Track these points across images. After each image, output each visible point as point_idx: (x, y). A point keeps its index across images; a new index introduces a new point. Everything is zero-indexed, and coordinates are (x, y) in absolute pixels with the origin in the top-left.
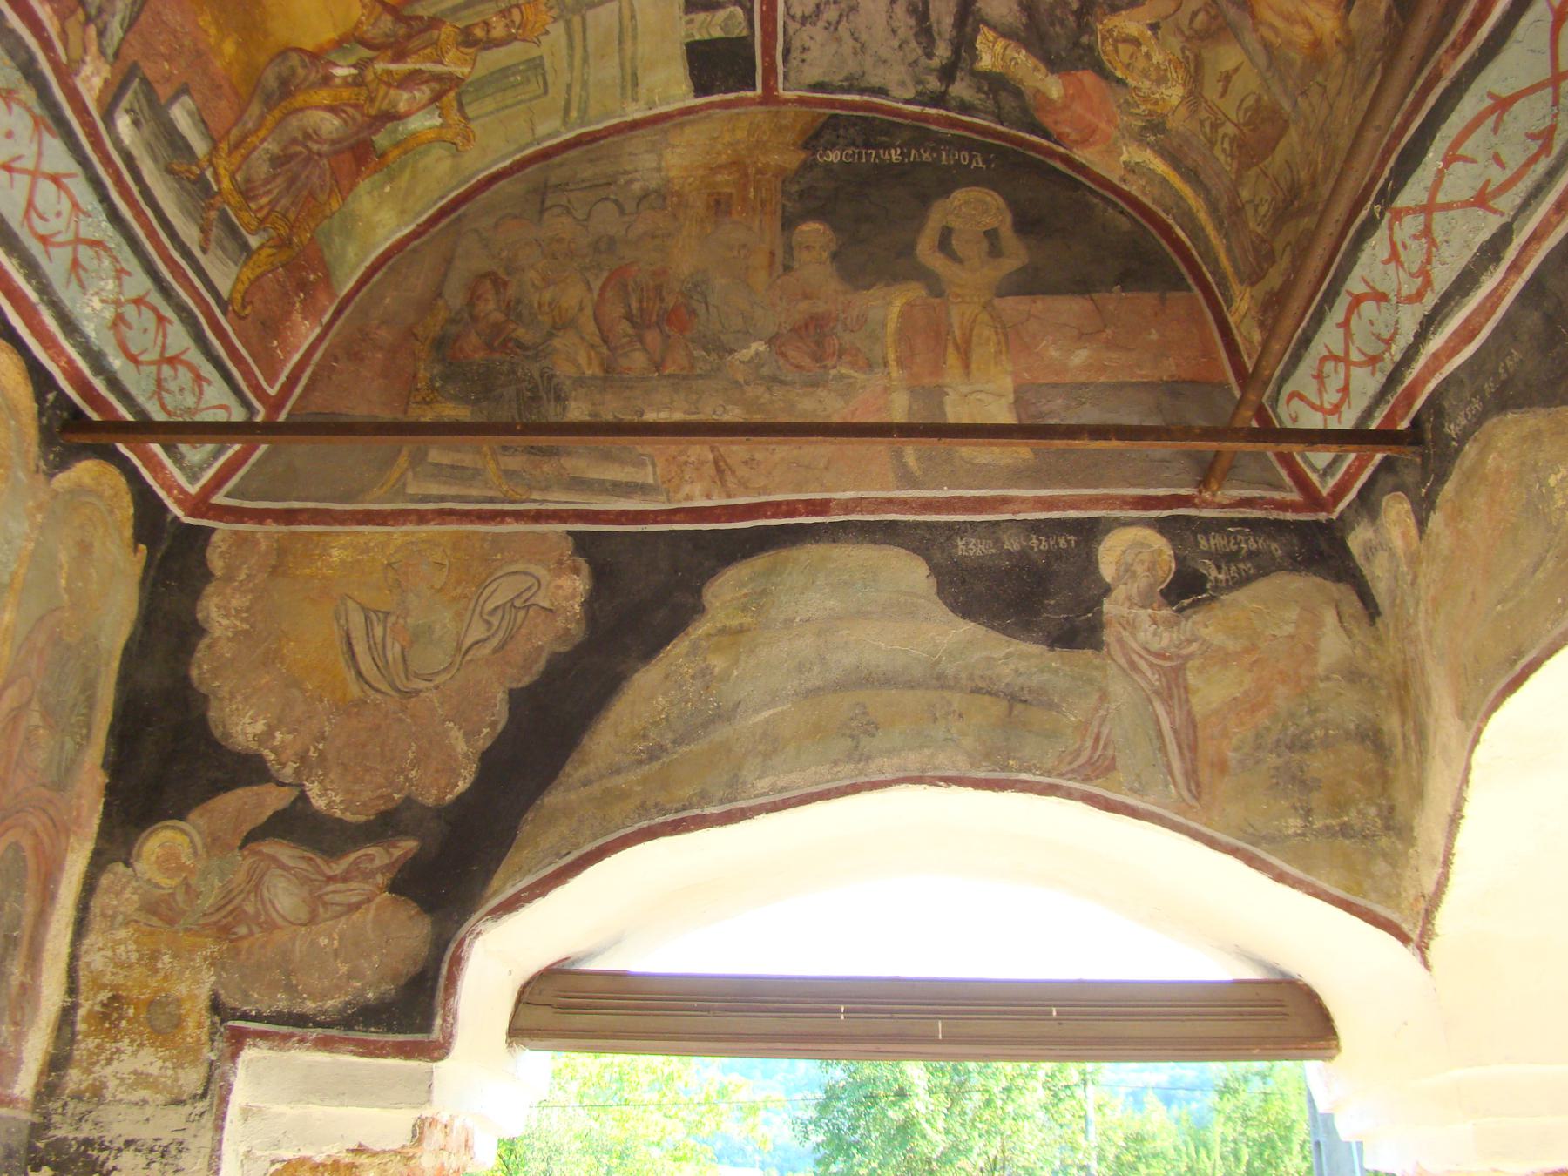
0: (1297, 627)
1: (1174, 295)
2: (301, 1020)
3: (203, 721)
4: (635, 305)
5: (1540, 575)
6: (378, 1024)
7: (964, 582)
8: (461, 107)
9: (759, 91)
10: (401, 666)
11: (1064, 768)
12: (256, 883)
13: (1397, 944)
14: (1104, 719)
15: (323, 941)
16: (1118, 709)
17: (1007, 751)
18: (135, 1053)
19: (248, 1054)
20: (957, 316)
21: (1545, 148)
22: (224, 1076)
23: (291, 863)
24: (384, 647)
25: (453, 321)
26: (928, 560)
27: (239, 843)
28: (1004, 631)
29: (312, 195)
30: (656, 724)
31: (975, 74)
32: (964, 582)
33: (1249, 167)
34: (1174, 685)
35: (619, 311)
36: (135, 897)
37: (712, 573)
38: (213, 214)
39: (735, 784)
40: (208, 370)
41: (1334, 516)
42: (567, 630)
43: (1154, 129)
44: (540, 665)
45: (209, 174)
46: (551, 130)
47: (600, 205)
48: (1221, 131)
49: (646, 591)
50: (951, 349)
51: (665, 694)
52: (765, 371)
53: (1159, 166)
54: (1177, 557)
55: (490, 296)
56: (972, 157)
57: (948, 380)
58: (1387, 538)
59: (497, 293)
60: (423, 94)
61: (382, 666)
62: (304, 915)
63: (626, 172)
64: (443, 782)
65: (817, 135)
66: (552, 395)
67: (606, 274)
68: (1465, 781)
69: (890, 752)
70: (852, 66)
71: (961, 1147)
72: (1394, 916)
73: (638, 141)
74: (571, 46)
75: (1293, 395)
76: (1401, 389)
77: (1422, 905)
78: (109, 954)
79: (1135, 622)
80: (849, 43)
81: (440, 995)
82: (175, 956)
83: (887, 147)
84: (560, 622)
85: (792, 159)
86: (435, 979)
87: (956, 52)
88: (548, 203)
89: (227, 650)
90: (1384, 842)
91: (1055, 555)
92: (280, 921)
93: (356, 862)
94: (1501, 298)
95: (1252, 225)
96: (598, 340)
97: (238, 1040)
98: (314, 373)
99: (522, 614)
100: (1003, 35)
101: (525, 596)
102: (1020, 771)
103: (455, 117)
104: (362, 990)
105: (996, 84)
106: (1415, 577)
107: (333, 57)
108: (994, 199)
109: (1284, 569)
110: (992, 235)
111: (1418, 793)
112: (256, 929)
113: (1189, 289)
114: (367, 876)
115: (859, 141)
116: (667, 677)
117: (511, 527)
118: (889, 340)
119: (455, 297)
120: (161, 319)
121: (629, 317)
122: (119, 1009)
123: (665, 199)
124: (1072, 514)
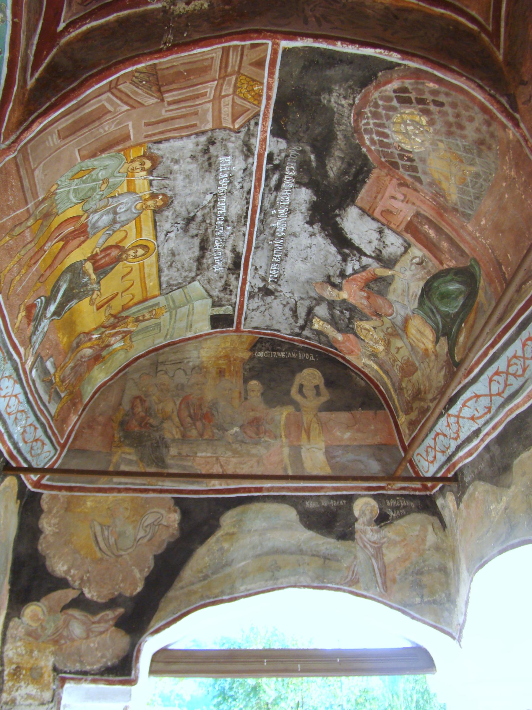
0: (419, 531)
1: (379, 412)
2: (85, 673)
3: (44, 565)
4: (192, 411)
5: (488, 535)
6: (112, 674)
7: (308, 517)
8: (131, 338)
9: (234, 328)
10: (115, 546)
11: (343, 582)
12: (67, 625)
13: (452, 639)
14: (355, 565)
15: (92, 645)
16: (360, 562)
17: (324, 575)
18: (26, 687)
19: (67, 685)
20: (307, 418)
21: (489, 411)
22: (59, 694)
23: (79, 617)
24: (108, 539)
25: (126, 415)
26: (296, 509)
27: (60, 610)
28: (322, 534)
29: (81, 375)
30: (205, 567)
31: (311, 329)
32: (308, 517)
33: (405, 377)
34: (378, 553)
35: (186, 414)
36: (23, 630)
37: (222, 513)
38: (53, 390)
39: (233, 589)
40: (47, 441)
41: (432, 493)
42: (173, 534)
43: (374, 355)
44: (164, 546)
45: (53, 378)
46: (160, 342)
47: (178, 371)
48: (396, 363)
49: (199, 521)
50: (303, 432)
51: (208, 556)
52: (239, 438)
53: (376, 367)
54: (379, 508)
55: (139, 405)
56: (310, 356)
57: (302, 443)
58: (447, 503)
59: (142, 405)
60: (119, 337)
61: (109, 546)
62: (84, 635)
63: (187, 358)
64: (132, 588)
65: (255, 346)
66: (164, 446)
67: (181, 399)
68: (469, 592)
69: (286, 577)
70: (268, 323)
71: (282, 697)
72: (450, 630)
73: (190, 346)
74: (171, 318)
75: (418, 454)
76: (451, 462)
77: (459, 627)
78: (15, 651)
79: (366, 531)
80: (268, 317)
81: (134, 662)
82: (39, 651)
83: (280, 351)
84: (171, 530)
85: (246, 355)
86: (132, 657)
87: (306, 322)
88: (159, 369)
89: (51, 539)
90: (447, 605)
91: (339, 507)
92: (76, 638)
93: (103, 617)
94: (479, 447)
95: (406, 395)
96: (179, 425)
97: (63, 681)
98: (76, 434)
99: (157, 527)
100: (323, 320)
101: (159, 520)
102: (328, 583)
103: (128, 341)
104: (106, 662)
105: (319, 333)
106: (456, 521)
107: (93, 333)
108: (317, 373)
109: (415, 512)
110: (317, 387)
111: (458, 591)
112: (68, 641)
113: (384, 409)
114: (106, 621)
115: (270, 348)
116: (208, 550)
117: (152, 495)
118: (282, 428)
119: (126, 406)
120: (36, 428)
121: (190, 416)
122: (20, 671)
123: (201, 370)
124: (345, 493)
